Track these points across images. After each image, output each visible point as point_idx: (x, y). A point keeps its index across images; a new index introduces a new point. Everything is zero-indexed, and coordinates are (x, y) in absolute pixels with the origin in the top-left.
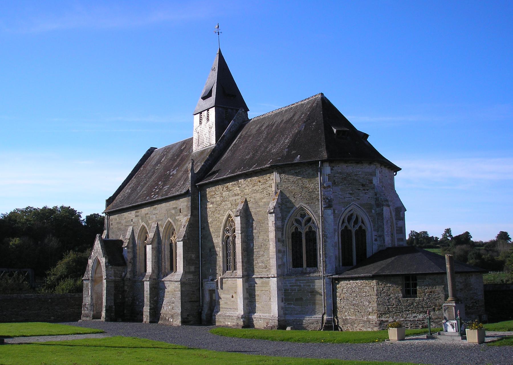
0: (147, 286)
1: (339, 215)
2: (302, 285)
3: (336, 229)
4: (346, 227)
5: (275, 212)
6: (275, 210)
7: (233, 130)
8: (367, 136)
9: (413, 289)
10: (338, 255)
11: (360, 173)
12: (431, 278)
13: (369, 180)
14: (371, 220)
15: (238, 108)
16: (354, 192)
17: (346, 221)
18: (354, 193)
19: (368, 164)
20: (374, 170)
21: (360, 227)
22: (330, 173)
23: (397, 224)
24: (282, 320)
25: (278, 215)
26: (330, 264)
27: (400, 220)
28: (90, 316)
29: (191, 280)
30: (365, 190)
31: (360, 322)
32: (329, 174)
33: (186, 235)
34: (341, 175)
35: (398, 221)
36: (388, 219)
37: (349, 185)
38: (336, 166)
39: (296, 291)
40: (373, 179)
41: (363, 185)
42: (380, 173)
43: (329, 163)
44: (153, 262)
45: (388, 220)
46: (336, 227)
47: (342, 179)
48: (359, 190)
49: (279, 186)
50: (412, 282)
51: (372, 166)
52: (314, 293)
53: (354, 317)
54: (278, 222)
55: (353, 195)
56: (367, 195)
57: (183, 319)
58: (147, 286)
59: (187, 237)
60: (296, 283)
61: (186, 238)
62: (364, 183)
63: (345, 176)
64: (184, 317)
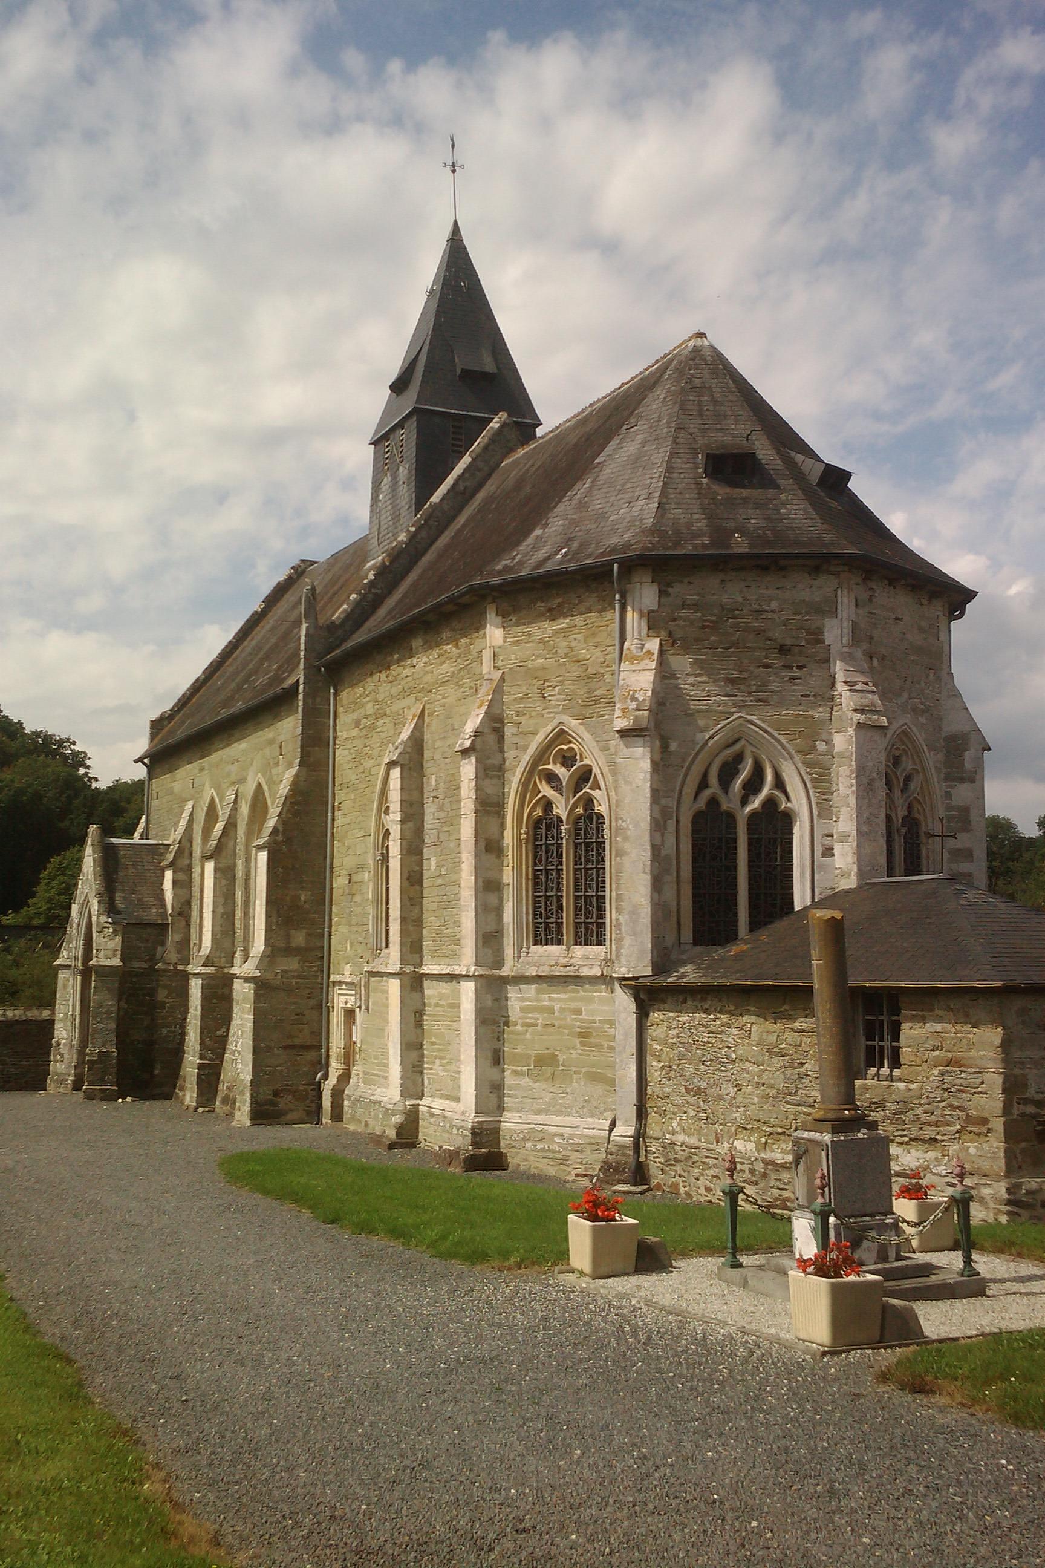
0: (195, 988)
1: (684, 760)
2: (557, 1007)
3: (671, 808)
4: (713, 802)
5: (478, 747)
6: (479, 739)
7: (466, 488)
8: (846, 476)
9: (881, 1043)
10: (675, 903)
11: (774, 605)
12: (952, 1006)
13: (809, 632)
14: (812, 780)
15: (492, 416)
16: (745, 675)
17: (713, 779)
18: (745, 678)
19: (810, 574)
20: (829, 594)
21: (713, 802)
22: (655, 607)
23: (948, 795)
24: (486, 1130)
25: (489, 758)
26: (635, 934)
27: (962, 780)
28: (67, 1080)
29: (293, 977)
30: (791, 668)
31: (707, 1160)
32: (653, 611)
33: (281, 829)
34: (699, 614)
35: (953, 787)
36: (875, 775)
37: (726, 648)
38: (682, 582)
39: (539, 1028)
40: (826, 629)
41: (783, 650)
42: (857, 605)
43: (653, 570)
44: (219, 916)
45: (873, 780)
46: (672, 803)
47: (704, 627)
48: (767, 666)
49: (501, 658)
50: (881, 1018)
51: (823, 579)
52: (592, 1040)
53: (693, 1141)
54: (487, 782)
55: (742, 687)
56: (797, 684)
57: (257, 1102)
58: (195, 988)
59: (283, 834)
60: (537, 1000)
61: (280, 838)
62: (788, 642)
63: (714, 618)
64: (261, 1096)
